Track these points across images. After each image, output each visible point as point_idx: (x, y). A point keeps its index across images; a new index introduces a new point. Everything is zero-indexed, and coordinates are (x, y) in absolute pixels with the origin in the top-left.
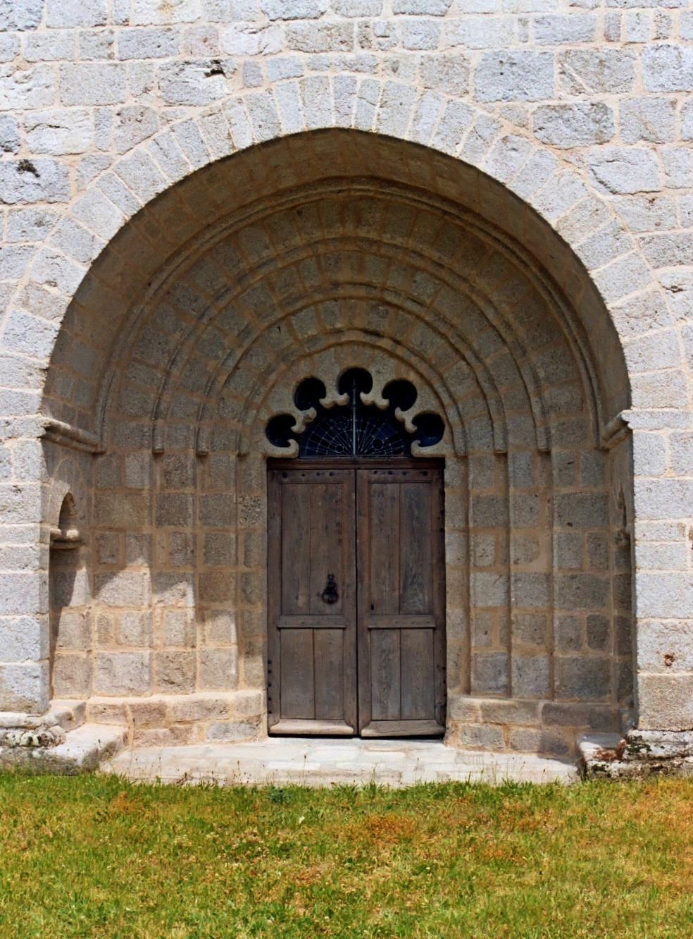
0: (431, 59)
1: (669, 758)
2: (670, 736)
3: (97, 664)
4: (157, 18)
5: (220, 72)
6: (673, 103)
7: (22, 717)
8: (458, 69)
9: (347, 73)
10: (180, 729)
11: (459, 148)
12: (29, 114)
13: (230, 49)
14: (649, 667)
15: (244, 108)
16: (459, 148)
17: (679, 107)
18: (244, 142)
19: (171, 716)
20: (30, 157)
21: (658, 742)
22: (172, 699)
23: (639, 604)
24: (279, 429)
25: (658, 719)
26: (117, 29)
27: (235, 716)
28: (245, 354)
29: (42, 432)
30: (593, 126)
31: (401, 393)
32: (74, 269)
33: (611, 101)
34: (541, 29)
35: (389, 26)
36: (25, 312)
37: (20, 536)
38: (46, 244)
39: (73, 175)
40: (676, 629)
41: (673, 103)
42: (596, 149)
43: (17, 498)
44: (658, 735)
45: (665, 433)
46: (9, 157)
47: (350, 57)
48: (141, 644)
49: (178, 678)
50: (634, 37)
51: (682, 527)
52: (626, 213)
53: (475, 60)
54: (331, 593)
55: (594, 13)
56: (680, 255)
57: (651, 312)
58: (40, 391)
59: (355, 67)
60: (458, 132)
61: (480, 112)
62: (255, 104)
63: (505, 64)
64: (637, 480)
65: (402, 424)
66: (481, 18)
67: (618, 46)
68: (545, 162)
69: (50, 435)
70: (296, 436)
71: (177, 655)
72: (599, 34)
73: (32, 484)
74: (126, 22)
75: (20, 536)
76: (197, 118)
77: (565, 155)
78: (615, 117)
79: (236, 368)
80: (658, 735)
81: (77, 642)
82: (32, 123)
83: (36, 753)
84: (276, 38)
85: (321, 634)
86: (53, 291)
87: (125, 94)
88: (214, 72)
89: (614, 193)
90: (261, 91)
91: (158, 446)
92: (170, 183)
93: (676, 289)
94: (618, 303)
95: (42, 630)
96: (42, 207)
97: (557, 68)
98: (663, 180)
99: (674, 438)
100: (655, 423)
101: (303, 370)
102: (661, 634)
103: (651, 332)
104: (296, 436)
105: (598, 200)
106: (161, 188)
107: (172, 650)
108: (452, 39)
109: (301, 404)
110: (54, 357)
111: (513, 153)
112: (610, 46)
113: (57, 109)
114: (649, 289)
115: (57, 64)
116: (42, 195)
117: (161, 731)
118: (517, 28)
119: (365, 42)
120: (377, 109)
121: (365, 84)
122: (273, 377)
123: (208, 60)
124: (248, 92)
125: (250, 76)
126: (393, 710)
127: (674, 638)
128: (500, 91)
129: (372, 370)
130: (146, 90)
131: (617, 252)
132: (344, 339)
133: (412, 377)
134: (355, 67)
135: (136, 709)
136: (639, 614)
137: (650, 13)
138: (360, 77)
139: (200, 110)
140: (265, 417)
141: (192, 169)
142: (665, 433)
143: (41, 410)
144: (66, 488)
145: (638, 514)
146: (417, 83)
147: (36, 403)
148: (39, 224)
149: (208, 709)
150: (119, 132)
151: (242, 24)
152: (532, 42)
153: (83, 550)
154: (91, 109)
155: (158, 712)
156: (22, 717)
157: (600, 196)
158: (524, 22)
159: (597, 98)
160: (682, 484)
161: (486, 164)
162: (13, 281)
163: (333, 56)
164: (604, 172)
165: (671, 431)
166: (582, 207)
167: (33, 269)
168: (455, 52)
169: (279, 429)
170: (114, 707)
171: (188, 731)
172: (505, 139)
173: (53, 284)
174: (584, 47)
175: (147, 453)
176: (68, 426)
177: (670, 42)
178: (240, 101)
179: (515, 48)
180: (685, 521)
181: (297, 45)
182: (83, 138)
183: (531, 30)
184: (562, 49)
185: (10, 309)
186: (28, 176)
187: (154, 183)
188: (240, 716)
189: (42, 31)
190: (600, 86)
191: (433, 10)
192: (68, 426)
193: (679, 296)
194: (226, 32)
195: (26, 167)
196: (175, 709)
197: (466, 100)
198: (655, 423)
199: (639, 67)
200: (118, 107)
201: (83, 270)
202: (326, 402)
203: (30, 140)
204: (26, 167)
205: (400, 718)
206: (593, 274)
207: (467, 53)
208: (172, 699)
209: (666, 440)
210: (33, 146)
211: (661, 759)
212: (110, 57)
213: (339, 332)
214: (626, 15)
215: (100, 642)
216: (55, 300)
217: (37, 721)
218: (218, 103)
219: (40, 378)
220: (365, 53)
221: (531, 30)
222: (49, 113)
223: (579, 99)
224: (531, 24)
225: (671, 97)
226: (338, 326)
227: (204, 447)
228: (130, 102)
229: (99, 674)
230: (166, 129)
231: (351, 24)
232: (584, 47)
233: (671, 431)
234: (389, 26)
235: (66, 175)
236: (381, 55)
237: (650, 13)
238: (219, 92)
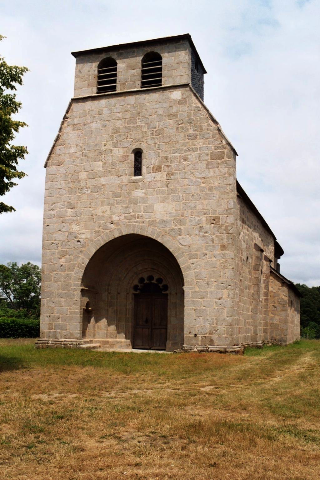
0: (150, 220)
1: (188, 350)
2: (189, 346)
3: (96, 333)
4: (102, 214)
5: (112, 223)
6: (194, 228)
7: (76, 340)
8: (154, 222)
9: (135, 223)
10: (112, 345)
11: (154, 237)
12: (79, 232)
13: (114, 219)
14: (186, 334)
15: (116, 230)
16: (154, 237)
17: (195, 228)
18: (116, 236)
19: (110, 343)
20: (79, 239)
21: (187, 347)
22: (110, 340)
23: (185, 323)
24: (136, 288)
25: (188, 343)
26: (95, 216)
27: (123, 344)
28: (127, 274)
29: (81, 290)
30: (179, 232)
31: (160, 280)
32: (87, 261)
33: (182, 228)
34: (170, 215)
35: (142, 215)
36: (78, 268)
37: (76, 309)
38: (82, 256)
39: (87, 243)
40: (191, 327)
41: (194, 228)
42: (179, 237)
43: (76, 302)
44: (187, 346)
45: (190, 291)
46: (76, 239)
47: (135, 220)
48: (105, 330)
49: (112, 336)
50: (187, 216)
51: (193, 309)
52: (184, 249)
53: (158, 220)
54: (147, 321)
55: (179, 212)
56: (194, 257)
57: (188, 268)
58: (80, 283)
59: (136, 222)
60: (154, 234)
61: (158, 230)
62: (118, 229)
63: (163, 221)
64: (185, 300)
65: (160, 287)
66: (159, 213)
67: (184, 217)
68: (170, 239)
69: (82, 291)
70: (139, 289)
71: (112, 332)
72: (180, 215)
73: (79, 299)
74: (96, 215)
75: (76, 309)
76: (108, 232)
77: (173, 238)
78: (183, 231)
79: (126, 276)
80: (187, 346)
81: (92, 329)
82: (80, 233)
83: (77, 346)
84: (122, 218)
85: (144, 329)
86: (83, 265)
87: (96, 228)
88: (111, 224)
89: (182, 245)
90: (119, 227)
91: (109, 292)
92: (103, 244)
93: (193, 264)
94: (182, 267)
95: (80, 326)
96: (82, 249)
97: (172, 222)
98: (191, 242)
99: (192, 292)
100: (189, 289)
101: (140, 276)
102: (188, 328)
103: (188, 272)
104: (139, 289)
105: (179, 247)
106: (102, 245)
107: (112, 331)
108: (154, 217)
109: (157, 280)
110: (83, 276)
111: (164, 238)
112: (182, 217)
113: (84, 231)
114: (188, 264)
115: (84, 222)
116: (81, 246)
117: (108, 346)
118: (165, 215)
119: (138, 218)
120: (140, 230)
121: (138, 225)
122: (134, 278)
123: (110, 221)
124: (117, 227)
125: (117, 224)
126: (158, 344)
127: (191, 329)
128: (162, 226)
129: (154, 276)
130: (100, 227)
131: (182, 257)
132: (148, 270)
133: (162, 277)
134: (136, 222)
135: (102, 341)
136: (185, 324)
137: (190, 211)
138: (137, 224)
139: (108, 230)
140: (133, 285)
141: (107, 241)
142: (190, 291)
143: (81, 286)
144: (88, 300)
145: (185, 306)
146: (147, 225)
147: (80, 285)
148: (81, 252)
149: (118, 342)
150: (95, 235)
151: (117, 215)
152: (168, 217)
153: (93, 312)
154: (90, 231)
155: (108, 342)
156: (76, 340)
157: (180, 246)
158: (167, 213)
159: (180, 227)
160: (193, 300)
161: (159, 240)
162: (76, 263)
163: (132, 220)
164: (181, 241)
165: (191, 291)
166: (176, 248)
167: (80, 261)
168: (154, 219)
169: (136, 288)
170: (98, 341)
171: (114, 346)
172: (163, 235)
173: (83, 263)
174: (177, 218)
175: (107, 293)
176: (87, 289)
177: (194, 216)
178: (116, 229)
179: (165, 218)
180: (194, 307)
181: (126, 218)
182: (89, 236)
183: (168, 215)
184: (173, 218)
185: (76, 268)
186: (79, 243)
187: (101, 244)
188: (125, 344)
189: (82, 217)
190: (181, 225)
191: (150, 212)
192: (87, 289)
193: (194, 265)
194: (114, 216)
195: (79, 241)
196: (111, 342)
197: (156, 228)
198: (189, 289)
199: (187, 221)
200: (95, 230)
201: (88, 261)
202: (145, 282)
203: (79, 236)
204: (79, 241)
205: (159, 346)
206: (178, 261)
207: (156, 219)
208: (110, 340)
209: (191, 292)
210: (80, 237)
211: (186, 350)
212: (93, 221)
213: (147, 269)
214: (185, 212)
215: (97, 329)
216: (84, 266)
217: (78, 341)
218: (112, 229)
219: (80, 280)
220: (138, 220)
221: (168, 215)
222: (84, 231)
223: (176, 227)
224: (168, 214)
225: (193, 227)
226: (146, 267)
227: (119, 292)
228: (97, 229)
229: (97, 335)
230: (103, 234)
231: (136, 215)
232: (177, 218)
233: (191, 291)
234: (142, 215)
235: (85, 243)
236: (141, 220)
237: (190, 211)
238: (112, 227)
